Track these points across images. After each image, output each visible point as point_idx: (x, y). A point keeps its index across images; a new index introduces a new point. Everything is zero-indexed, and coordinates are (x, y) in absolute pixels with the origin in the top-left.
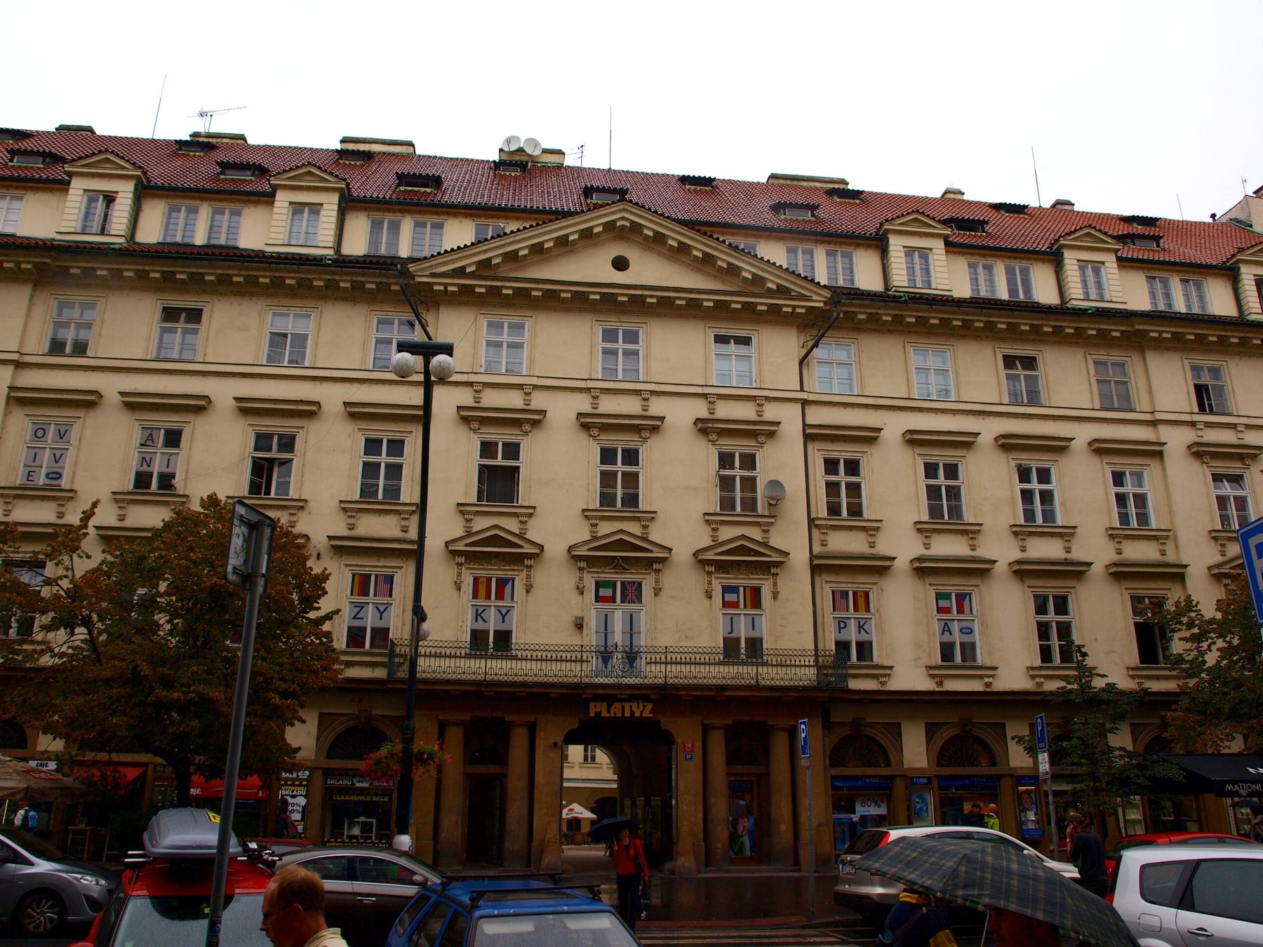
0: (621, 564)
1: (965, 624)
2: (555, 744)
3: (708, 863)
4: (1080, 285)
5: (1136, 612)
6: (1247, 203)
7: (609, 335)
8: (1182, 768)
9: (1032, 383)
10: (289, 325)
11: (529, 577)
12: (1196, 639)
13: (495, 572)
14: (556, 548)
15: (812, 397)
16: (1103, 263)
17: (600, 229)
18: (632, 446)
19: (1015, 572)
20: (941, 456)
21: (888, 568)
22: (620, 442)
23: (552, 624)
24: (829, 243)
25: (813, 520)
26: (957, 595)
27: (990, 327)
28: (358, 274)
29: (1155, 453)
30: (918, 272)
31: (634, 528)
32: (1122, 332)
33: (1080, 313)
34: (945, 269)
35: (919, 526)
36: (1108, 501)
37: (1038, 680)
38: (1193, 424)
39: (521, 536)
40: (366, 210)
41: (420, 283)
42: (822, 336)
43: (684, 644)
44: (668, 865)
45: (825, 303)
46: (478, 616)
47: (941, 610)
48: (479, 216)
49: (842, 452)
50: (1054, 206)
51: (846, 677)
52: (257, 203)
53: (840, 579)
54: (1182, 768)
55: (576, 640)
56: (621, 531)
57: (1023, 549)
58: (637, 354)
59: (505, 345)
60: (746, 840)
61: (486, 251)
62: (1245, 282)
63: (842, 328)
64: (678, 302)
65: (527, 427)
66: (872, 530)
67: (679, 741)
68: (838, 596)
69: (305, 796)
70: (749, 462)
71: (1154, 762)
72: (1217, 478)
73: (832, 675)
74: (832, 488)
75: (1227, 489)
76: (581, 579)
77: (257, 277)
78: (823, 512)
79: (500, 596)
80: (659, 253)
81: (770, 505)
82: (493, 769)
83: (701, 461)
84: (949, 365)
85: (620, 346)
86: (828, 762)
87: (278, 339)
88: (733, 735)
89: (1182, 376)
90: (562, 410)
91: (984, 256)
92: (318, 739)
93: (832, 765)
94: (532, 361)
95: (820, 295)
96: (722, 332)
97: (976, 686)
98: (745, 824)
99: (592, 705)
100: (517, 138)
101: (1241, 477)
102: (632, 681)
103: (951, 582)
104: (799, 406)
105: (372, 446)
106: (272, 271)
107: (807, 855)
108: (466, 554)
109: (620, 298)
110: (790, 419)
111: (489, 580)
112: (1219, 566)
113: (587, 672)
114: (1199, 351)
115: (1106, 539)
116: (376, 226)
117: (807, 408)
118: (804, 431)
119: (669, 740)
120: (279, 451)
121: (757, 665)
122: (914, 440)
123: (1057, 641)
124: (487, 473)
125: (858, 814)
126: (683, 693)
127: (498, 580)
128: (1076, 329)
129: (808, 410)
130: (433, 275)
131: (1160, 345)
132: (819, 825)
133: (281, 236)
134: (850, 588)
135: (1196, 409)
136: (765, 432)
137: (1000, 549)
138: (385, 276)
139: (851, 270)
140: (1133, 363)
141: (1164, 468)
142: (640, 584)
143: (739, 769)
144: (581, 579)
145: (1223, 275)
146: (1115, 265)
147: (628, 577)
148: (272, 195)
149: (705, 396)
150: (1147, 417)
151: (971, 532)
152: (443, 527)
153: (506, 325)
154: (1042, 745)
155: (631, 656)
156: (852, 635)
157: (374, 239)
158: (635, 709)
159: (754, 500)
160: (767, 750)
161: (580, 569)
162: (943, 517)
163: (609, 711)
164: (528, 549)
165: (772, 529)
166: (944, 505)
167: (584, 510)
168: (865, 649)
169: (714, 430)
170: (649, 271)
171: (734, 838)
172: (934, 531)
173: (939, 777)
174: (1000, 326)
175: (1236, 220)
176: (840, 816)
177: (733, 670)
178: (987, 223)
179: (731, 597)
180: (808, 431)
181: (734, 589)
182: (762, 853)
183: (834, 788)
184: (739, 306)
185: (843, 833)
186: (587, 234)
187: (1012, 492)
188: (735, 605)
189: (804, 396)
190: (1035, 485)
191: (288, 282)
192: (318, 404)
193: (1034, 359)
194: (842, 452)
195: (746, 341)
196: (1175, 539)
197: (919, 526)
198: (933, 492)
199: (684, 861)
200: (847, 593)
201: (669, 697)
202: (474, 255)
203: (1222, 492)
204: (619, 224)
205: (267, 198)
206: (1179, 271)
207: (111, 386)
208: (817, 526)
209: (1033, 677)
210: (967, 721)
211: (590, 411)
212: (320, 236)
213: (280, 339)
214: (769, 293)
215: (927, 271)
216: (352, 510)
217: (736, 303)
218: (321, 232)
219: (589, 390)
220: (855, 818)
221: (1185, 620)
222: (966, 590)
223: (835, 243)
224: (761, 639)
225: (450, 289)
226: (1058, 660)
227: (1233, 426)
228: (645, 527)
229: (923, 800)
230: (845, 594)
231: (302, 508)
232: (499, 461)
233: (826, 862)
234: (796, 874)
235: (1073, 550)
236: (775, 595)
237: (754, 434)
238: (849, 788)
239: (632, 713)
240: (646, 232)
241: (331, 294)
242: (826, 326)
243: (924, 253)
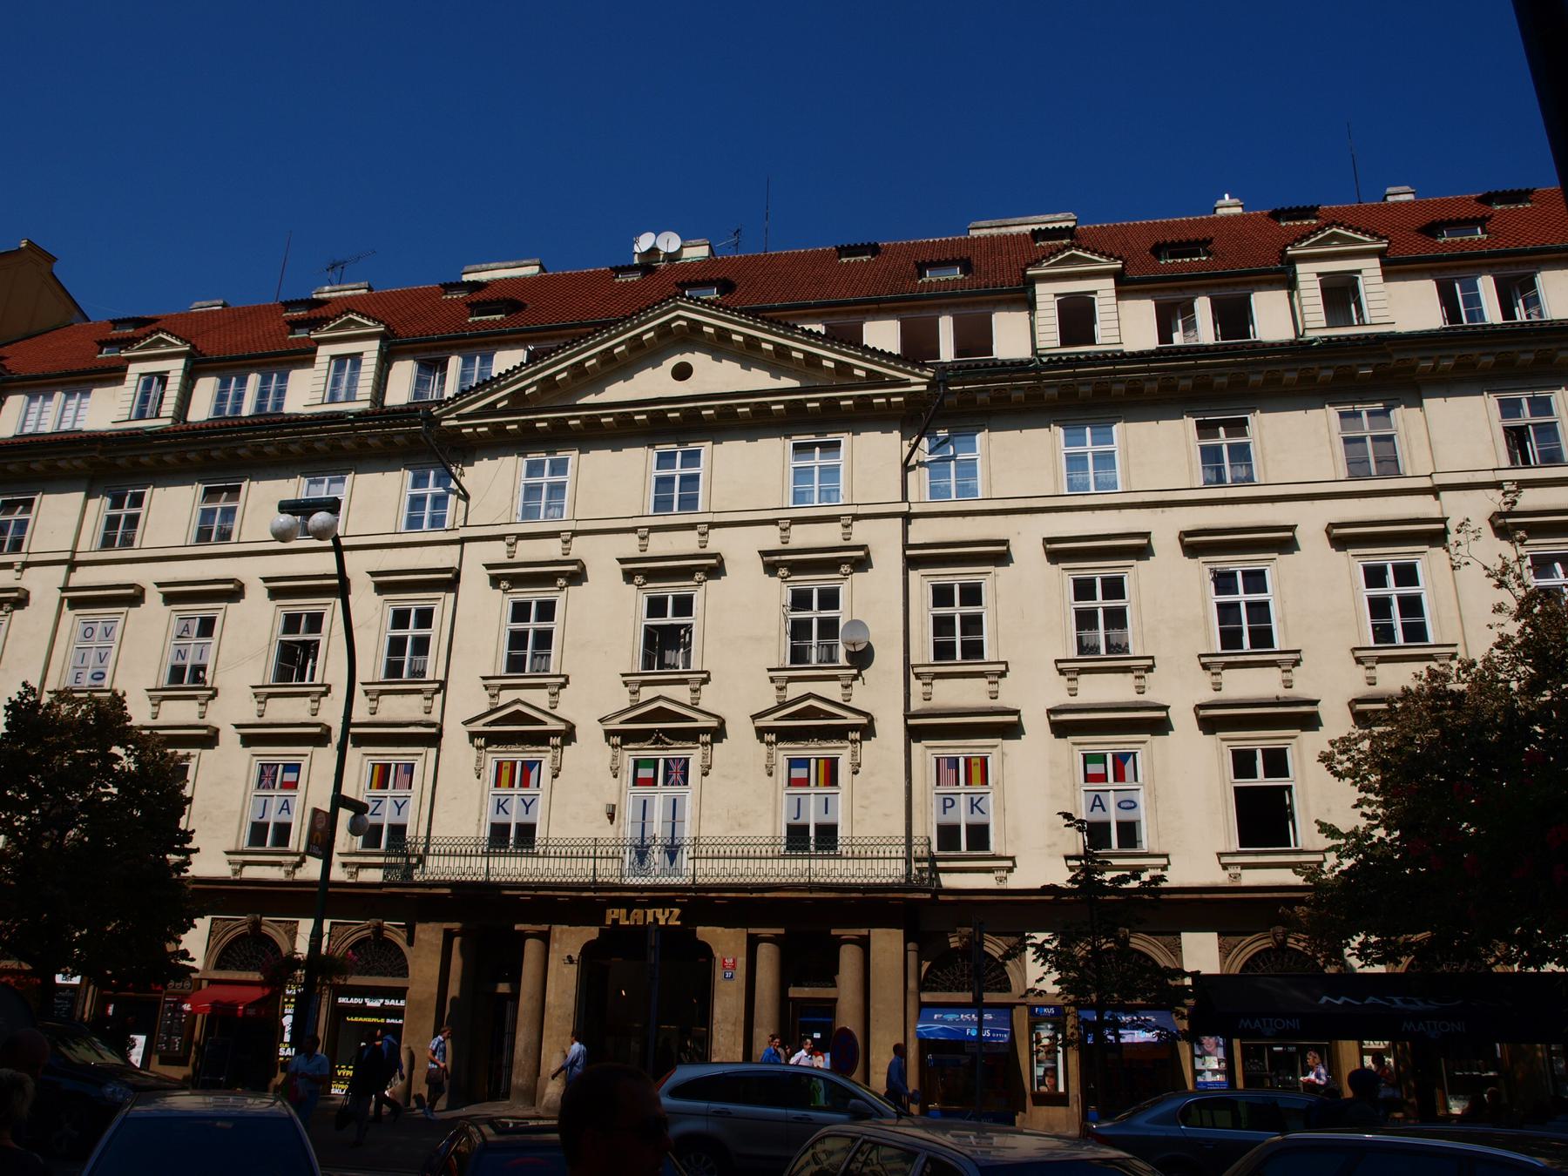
1: (1125, 796)
16: (1359, 272)
37: (1232, 870)
43: (734, 834)
46: (500, 806)
56: (810, 696)
57: (1073, 692)
58: (1113, 457)
68: (944, 764)
70: (830, 599)
94: (1127, 471)
102: (674, 880)
105: (1083, 589)
110: (884, 541)
111: (514, 764)
120: (675, 614)
122: (1058, 552)
127: (1115, 756)
129: (916, 525)
134: (393, 761)
135: (1506, 463)
142: (687, 760)
150: (1426, 483)
152: (233, 708)
155: (672, 851)
157: (421, 383)
158: (659, 916)
160: (834, 968)
164: (553, 725)
177: (802, 864)
178: (1210, 242)
181: (804, 763)
187: (1205, 606)
188: (805, 782)
190: (1392, 590)
200: (957, 760)
207: (250, 572)
208: (918, 676)
209: (1225, 867)
211: (639, 554)
216: (1071, 671)
217: (813, 401)
222: (1127, 748)
239: (656, 920)
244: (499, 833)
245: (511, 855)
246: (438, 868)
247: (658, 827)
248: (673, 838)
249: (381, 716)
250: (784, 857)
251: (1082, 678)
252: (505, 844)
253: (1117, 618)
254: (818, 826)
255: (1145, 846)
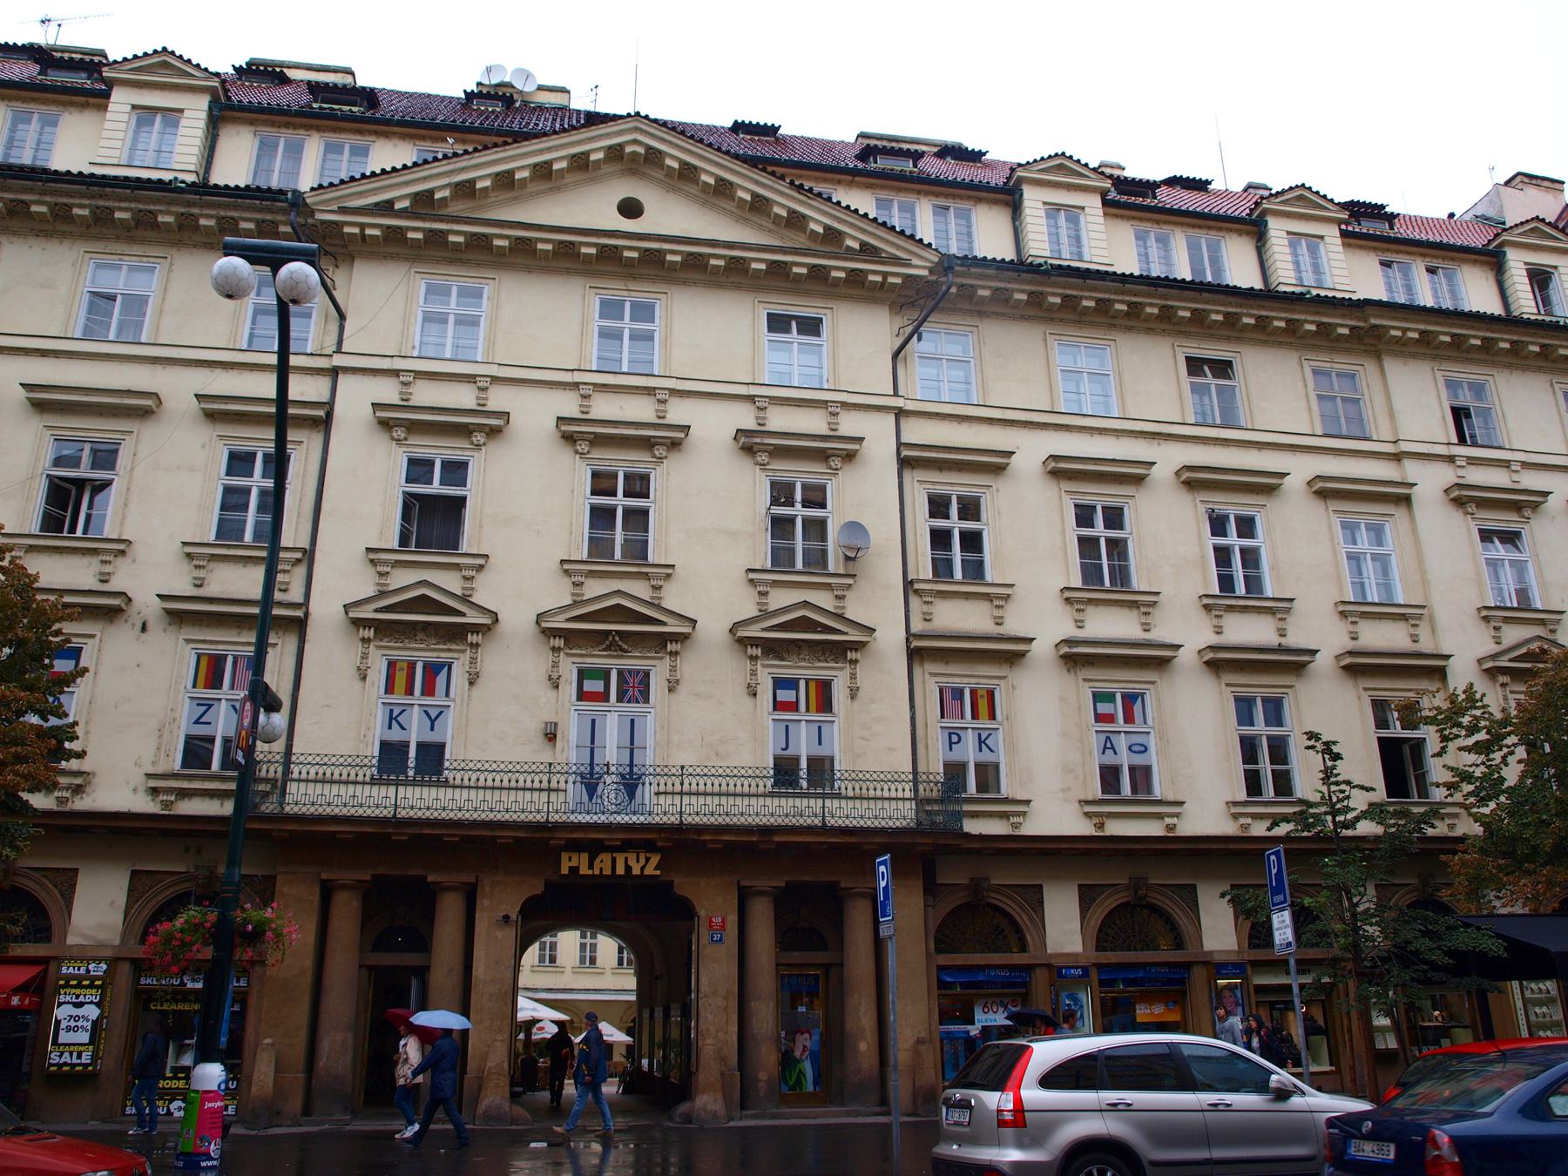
0: (617, 641)
2: (506, 918)
3: (745, 1102)
4: (1291, 266)
5: (1381, 723)
6: (1498, 194)
7: (610, 309)
8: (1499, 936)
9: (1227, 396)
10: (118, 281)
11: (473, 661)
12: (1482, 748)
13: (421, 653)
14: (517, 617)
15: (910, 406)
16: (1322, 237)
17: (600, 155)
18: (640, 469)
19: (1208, 663)
20: (1100, 496)
21: (1022, 654)
22: (622, 462)
23: (510, 735)
24: (937, 195)
25: (912, 582)
26: (1124, 696)
27: (1167, 315)
28: (228, 207)
29: (1401, 499)
30: (1064, 239)
31: (640, 589)
32: (1352, 328)
33: (1295, 300)
34: (1104, 236)
35: (1068, 594)
36: (1337, 564)
37: (1243, 821)
38: (1451, 459)
39: (464, 599)
40: (251, 123)
41: (323, 222)
42: (924, 320)
44: (683, 1108)
45: (931, 271)
47: (1100, 718)
48: (423, 138)
49: (955, 485)
50: (1245, 190)
51: (960, 816)
52: (84, 106)
53: (951, 669)
54: (1499, 936)
55: (546, 756)
56: (618, 593)
57: (1080, 624)
58: (652, 339)
59: (451, 319)
60: (807, 1067)
61: (425, 179)
62: (1514, 271)
63: (954, 310)
64: (713, 262)
65: (479, 438)
66: (999, 598)
67: (702, 913)
68: (948, 696)
69: (98, 1005)
70: (816, 497)
71: (1449, 928)
72: (1486, 536)
73: (938, 813)
74: (940, 539)
75: (1499, 550)
76: (555, 665)
77: (70, 207)
78: (927, 572)
79: (429, 690)
80: (687, 195)
81: (848, 558)
82: (411, 959)
83: (744, 495)
84: (1109, 367)
85: (627, 324)
86: (932, 945)
87: (102, 300)
88: (787, 903)
89: (1434, 393)
90: (533, 415)
91: (1157, 222)
92: (126, 913)
93: (939, 950)
94: (491, 343)
95: (922, 258)
96: (779, 310)
97: (1153, 829)
98: (805, 1043)
99: (565, 857)
100: (501, 68)
101: (1517, 535)
103: (1119, 674)
104: (891, 418)
105: (602, 483)
106: (93, 197)
107: (900, 1089)
108: (379, 625)
109: (627, 254)
110: (878, 437)
111: (412, 666)
112: (1494, 657)
113: (565, 805)
114: (1456, 360)
115: (1336, 618)
116: (266, 150)
117: (903, 421)
118: (898, 453)
119: (686, 911)
121: (824, 796)
122: (1060, 470)
123: (1264, 764)
124: (412, 504)
125: (978, 1025)
126: (708, 838)
128: (1288, 321)
129: (904, 424)
130: (343, 210)
131: (1405, 349)
132: (920, 1041)
133: (117, 153)
134: (967, 683)
136: (838, 452)
137: (1186, 629)
138: (270, 211)
139: (970, 235)
140: (1367, 372)
141: (1412, 520)
142: (647, 674)
143: (797, 957)
144: (555, 665)
145: (1482, 263)
146: (1339, 241)
147: (629, 663)
148: (106, 95)
149: (751, 399)
150: (1389, 448)
151: (1143, 604)
152: (339, 581)
153: (455, 289)
154: (1280, 898)
155: (631, 783)
156: (969, 752)
158: (632, 863)
159: (824, 552)
161: (554, 649)
162: (1102, 584)
163: (591, 866)
164: (473, 618)
165: (850, 595)
166: (1104, 565)
167: (562, 562)
168: (988, 775)
169: (764, 448)
170: (671, 217)
171: (787, 1061)
172: (1090, 601)
173: (1099, 966)
174: (1181, 313)
175: (1482, 217)
176: (952, 1028)
177: (787, 804)
179: (786, 695)
180: (905, 453)
181: (791, 684)
182: (830, 1088)
183: (942, 985)
184: (804, 271)
185: (956, 1054)
186: (580, 163)
188: (793, 707)
189: (899, 402)
190: (1233, 540)
191: (118, 215)
192: (155, 396)
193: (1229, 364)
194: (955, 485)
195: (811, 327)
196: (1432, 620)
197: (1068, 594)
198: (1088, 546)
199: (708, 1102)
200: (961, 691)
201: (685, 845)
202: (407, 183)
203: (1493, 554)
204: (628, 149)
205: (96, 98)
206: (1423, 255)
209: (1235, 816)
210: (1139, 880)
212: (180, 155)
213: (102, 303)
214: (850, 254)
215: (1077, 239)
216: (201, 556)
218: (178, 149)
219: (575, 386)
220: (974, 1030)
221: (1466, 720)
222: (1137, 688)
223: (946, 196)
224: (832, 759)
225: (368, 232)
226: (1272, 793)
227: (1506, 464)
228: (657, 588)
229: (1076, 1001)
230: (958, 693)
231: (123, 552)
232: (436, 488)
233: (927, 1099)
234: (881, 1119)
235: (1290, 633)
236: (854, 693)
237: (823, 456)
238: (964, 985)
239: (628, 868)
240: (669, 162)
241: (186, 236)
242: (931, 303)
243: (1073, 212)
244: (392, 754)
245: (802, 795)
246: (303, 798)
247: (611, 752)
248: (631, 765)
249: (212, 589)
250: (771, 795)
251: (1090, 610)
252: (794, 783)
253: (638, 518)
254: (420, 745)
255: (1158, 793)
